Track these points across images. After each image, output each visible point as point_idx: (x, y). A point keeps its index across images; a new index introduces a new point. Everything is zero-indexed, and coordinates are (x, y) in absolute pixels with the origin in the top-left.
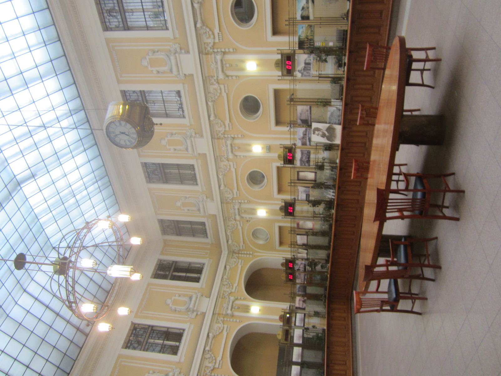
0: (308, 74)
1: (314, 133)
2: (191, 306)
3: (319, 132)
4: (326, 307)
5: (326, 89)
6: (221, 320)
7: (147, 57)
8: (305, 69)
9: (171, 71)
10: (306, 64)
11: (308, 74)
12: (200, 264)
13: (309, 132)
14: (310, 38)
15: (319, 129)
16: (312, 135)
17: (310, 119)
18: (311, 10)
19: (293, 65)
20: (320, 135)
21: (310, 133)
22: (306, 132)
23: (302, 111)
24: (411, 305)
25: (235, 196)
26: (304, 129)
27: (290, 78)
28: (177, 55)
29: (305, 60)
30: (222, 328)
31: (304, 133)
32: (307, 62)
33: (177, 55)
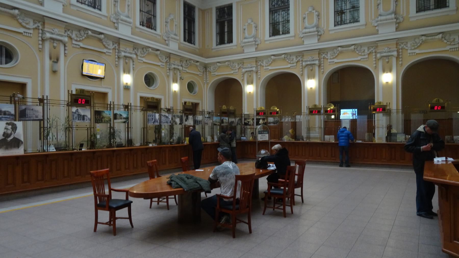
0: (75, 118)
1: (7, 124)
2: (122, 17)
3: (11, 130)
4: (410, 142)
5: (59, 136)
6: (38, 26)
7: (253, 23)
8: (79, 115)
9: (245, 38)
10: (84, 116)
11: (75, 118)
12: (194, 41)
13: (9, 118)
14: (103, 120)
15: (16, 130)
16: (5, 122)
17: (27, 119)
18: (120, 120)
19: (81, 106)
20: (5, 130)
21: (6, 119)
22: (9, 115)
23: (37, 111)
24: (105, 222)
25: (212, 73)
26: (13, 112)
27: (255, 114)
28: (254, 43)
29: (86, 116)
30: (27, 26)
31: (7, 113)
32: (85, 117)
33: (254, 43)
